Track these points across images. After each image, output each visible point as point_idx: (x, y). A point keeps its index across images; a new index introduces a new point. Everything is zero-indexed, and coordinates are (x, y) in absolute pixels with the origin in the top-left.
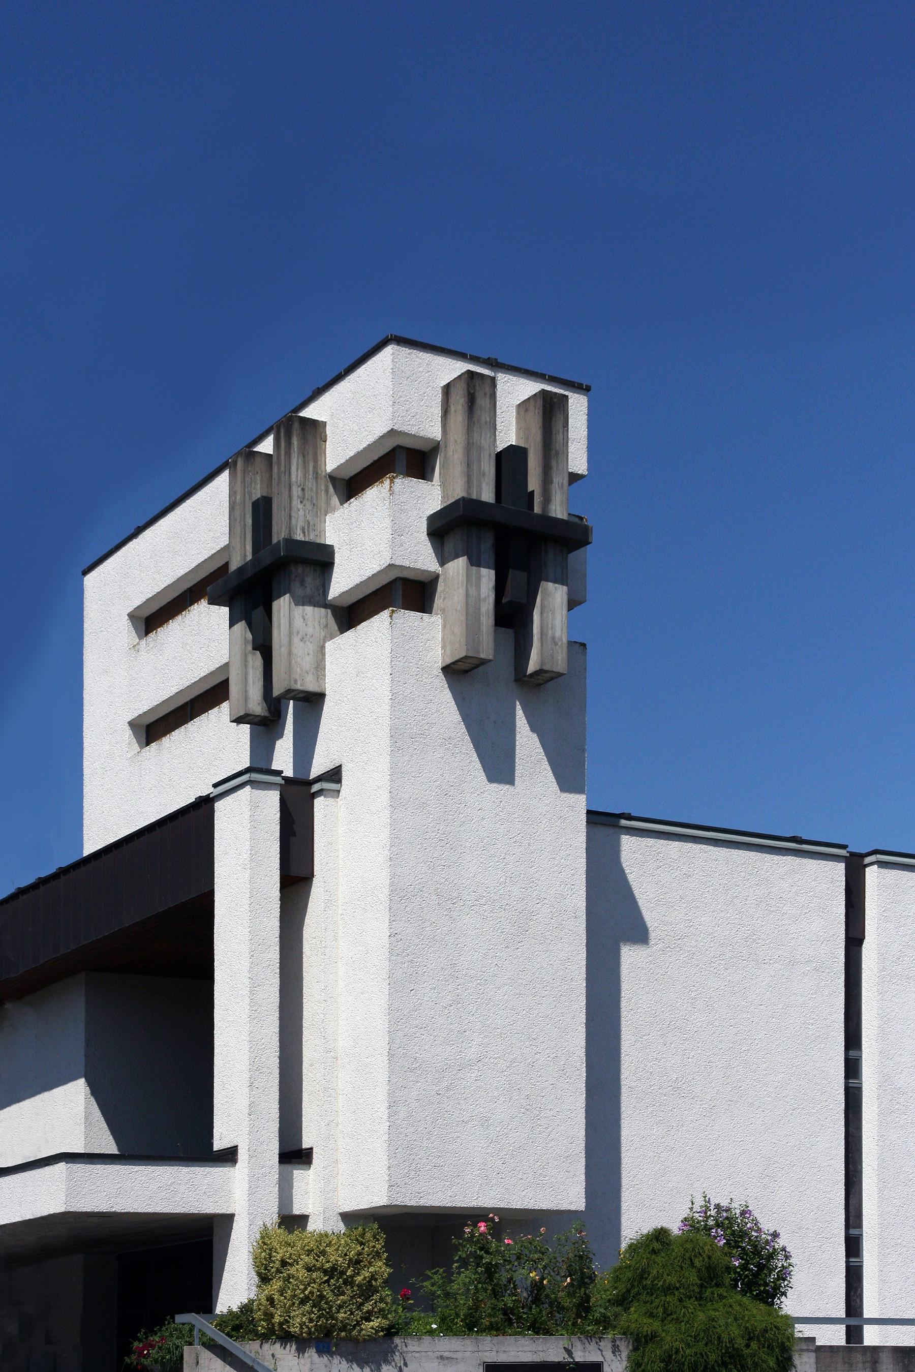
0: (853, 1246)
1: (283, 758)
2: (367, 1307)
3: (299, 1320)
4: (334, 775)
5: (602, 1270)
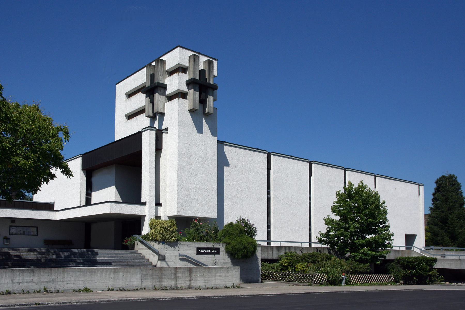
0: (269, 227)
1: (156, 125)
2: (172, 235)
3: (158, 237)
4: (167, 129)
5: (220, 230)
